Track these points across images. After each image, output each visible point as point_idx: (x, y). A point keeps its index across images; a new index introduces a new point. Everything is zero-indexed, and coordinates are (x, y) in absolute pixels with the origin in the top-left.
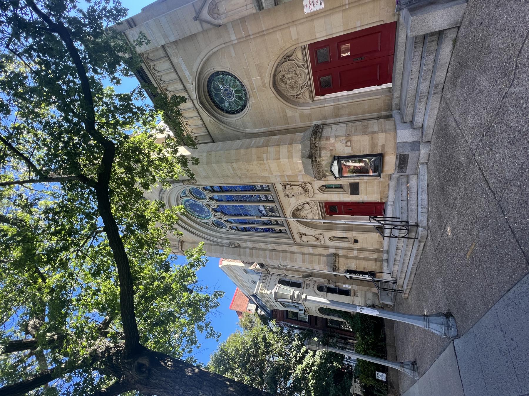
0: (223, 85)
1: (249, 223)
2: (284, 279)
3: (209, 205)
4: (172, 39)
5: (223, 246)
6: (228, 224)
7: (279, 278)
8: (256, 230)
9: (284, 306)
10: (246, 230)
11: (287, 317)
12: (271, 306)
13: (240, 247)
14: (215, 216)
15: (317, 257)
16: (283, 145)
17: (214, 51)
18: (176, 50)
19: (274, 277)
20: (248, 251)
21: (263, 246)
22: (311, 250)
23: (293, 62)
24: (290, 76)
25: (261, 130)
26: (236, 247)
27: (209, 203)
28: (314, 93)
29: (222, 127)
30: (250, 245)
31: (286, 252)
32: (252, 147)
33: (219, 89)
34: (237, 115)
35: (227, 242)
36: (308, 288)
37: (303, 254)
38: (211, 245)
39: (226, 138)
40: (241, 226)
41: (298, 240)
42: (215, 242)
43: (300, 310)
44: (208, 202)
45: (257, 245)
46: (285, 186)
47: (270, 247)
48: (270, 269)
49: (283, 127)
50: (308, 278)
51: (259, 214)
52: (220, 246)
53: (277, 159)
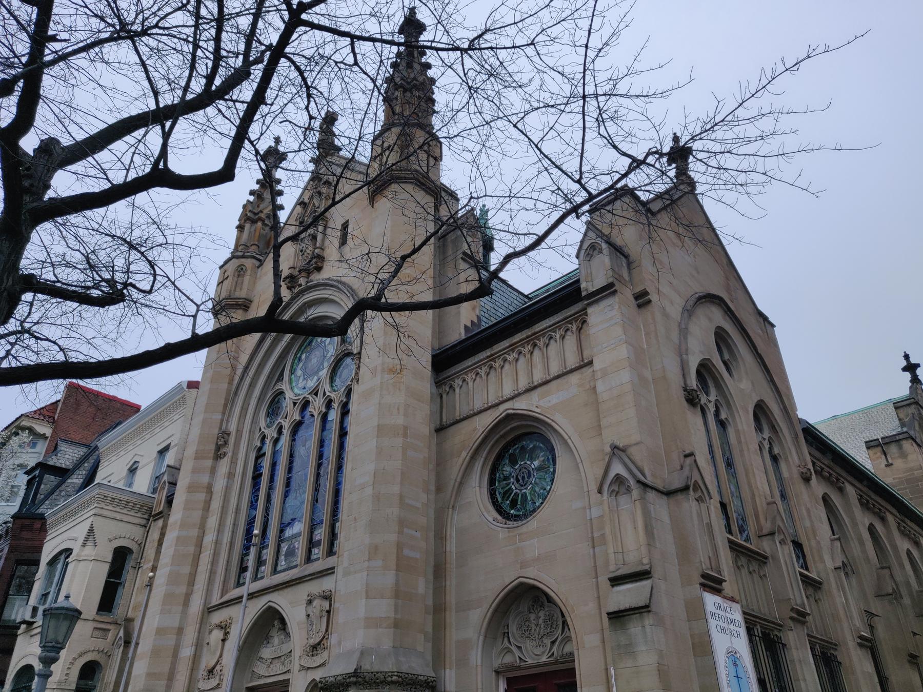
0: (539, 469)
1: (271, 487)
2: (130, 563)
3: (316, 394)
4: (600, 387)
5: (224, 414)
6: (271, 433)
7: (134, 547)
8: (253, 505)
9: (52, 562)
10: (257, 477)
11: (19, 562)
12: (58, 522)
13: (218, 455)
14: (295, 404)
15: (166, 669)
16: (396, 606)
17: (580, 465)
18: (588, 387)
19: (138, 533)
20: (205, 479)
21: (212, 522)
22: (187, 652)
23: (560, 631)
24: (541, 621)
25: (451, 546)
26: (218, 447)
27: (320, 394)
28: (511, 675)
29: (464, 454)
30: (219, 484)
31: (191, 582)
32: (400, 532)
33: (532, 459)
34: (485, 490)
35: (233, 428)
36: (97, 633)
37: (180, 631)
38: (234, 368)
39: (440, 462)
40: (266, 463)
41: (217, 617)
42: (236, 393)
43: (35, 610)
44: (325, 393)
45: (216, 504)
46: (327, 597)
47: (209, 539)
48: (160, 523)
49: (452, 598)
50: (121, 634)
51: (287, 519)
52: (225, 405)
53: (367, 592)
